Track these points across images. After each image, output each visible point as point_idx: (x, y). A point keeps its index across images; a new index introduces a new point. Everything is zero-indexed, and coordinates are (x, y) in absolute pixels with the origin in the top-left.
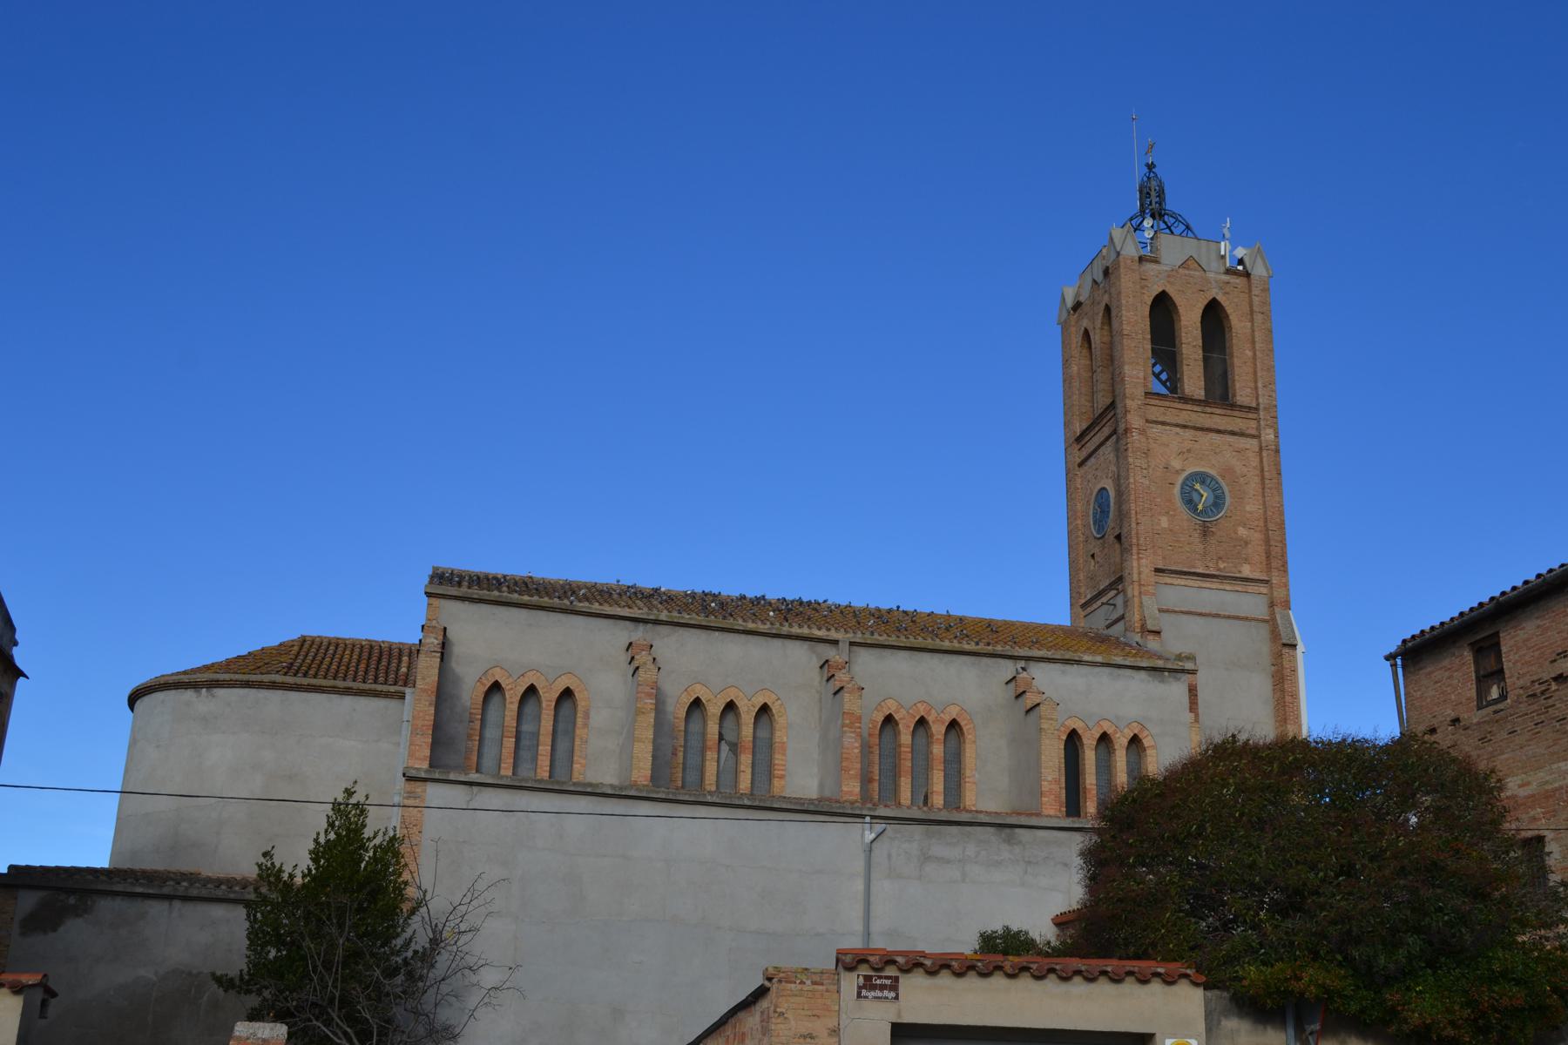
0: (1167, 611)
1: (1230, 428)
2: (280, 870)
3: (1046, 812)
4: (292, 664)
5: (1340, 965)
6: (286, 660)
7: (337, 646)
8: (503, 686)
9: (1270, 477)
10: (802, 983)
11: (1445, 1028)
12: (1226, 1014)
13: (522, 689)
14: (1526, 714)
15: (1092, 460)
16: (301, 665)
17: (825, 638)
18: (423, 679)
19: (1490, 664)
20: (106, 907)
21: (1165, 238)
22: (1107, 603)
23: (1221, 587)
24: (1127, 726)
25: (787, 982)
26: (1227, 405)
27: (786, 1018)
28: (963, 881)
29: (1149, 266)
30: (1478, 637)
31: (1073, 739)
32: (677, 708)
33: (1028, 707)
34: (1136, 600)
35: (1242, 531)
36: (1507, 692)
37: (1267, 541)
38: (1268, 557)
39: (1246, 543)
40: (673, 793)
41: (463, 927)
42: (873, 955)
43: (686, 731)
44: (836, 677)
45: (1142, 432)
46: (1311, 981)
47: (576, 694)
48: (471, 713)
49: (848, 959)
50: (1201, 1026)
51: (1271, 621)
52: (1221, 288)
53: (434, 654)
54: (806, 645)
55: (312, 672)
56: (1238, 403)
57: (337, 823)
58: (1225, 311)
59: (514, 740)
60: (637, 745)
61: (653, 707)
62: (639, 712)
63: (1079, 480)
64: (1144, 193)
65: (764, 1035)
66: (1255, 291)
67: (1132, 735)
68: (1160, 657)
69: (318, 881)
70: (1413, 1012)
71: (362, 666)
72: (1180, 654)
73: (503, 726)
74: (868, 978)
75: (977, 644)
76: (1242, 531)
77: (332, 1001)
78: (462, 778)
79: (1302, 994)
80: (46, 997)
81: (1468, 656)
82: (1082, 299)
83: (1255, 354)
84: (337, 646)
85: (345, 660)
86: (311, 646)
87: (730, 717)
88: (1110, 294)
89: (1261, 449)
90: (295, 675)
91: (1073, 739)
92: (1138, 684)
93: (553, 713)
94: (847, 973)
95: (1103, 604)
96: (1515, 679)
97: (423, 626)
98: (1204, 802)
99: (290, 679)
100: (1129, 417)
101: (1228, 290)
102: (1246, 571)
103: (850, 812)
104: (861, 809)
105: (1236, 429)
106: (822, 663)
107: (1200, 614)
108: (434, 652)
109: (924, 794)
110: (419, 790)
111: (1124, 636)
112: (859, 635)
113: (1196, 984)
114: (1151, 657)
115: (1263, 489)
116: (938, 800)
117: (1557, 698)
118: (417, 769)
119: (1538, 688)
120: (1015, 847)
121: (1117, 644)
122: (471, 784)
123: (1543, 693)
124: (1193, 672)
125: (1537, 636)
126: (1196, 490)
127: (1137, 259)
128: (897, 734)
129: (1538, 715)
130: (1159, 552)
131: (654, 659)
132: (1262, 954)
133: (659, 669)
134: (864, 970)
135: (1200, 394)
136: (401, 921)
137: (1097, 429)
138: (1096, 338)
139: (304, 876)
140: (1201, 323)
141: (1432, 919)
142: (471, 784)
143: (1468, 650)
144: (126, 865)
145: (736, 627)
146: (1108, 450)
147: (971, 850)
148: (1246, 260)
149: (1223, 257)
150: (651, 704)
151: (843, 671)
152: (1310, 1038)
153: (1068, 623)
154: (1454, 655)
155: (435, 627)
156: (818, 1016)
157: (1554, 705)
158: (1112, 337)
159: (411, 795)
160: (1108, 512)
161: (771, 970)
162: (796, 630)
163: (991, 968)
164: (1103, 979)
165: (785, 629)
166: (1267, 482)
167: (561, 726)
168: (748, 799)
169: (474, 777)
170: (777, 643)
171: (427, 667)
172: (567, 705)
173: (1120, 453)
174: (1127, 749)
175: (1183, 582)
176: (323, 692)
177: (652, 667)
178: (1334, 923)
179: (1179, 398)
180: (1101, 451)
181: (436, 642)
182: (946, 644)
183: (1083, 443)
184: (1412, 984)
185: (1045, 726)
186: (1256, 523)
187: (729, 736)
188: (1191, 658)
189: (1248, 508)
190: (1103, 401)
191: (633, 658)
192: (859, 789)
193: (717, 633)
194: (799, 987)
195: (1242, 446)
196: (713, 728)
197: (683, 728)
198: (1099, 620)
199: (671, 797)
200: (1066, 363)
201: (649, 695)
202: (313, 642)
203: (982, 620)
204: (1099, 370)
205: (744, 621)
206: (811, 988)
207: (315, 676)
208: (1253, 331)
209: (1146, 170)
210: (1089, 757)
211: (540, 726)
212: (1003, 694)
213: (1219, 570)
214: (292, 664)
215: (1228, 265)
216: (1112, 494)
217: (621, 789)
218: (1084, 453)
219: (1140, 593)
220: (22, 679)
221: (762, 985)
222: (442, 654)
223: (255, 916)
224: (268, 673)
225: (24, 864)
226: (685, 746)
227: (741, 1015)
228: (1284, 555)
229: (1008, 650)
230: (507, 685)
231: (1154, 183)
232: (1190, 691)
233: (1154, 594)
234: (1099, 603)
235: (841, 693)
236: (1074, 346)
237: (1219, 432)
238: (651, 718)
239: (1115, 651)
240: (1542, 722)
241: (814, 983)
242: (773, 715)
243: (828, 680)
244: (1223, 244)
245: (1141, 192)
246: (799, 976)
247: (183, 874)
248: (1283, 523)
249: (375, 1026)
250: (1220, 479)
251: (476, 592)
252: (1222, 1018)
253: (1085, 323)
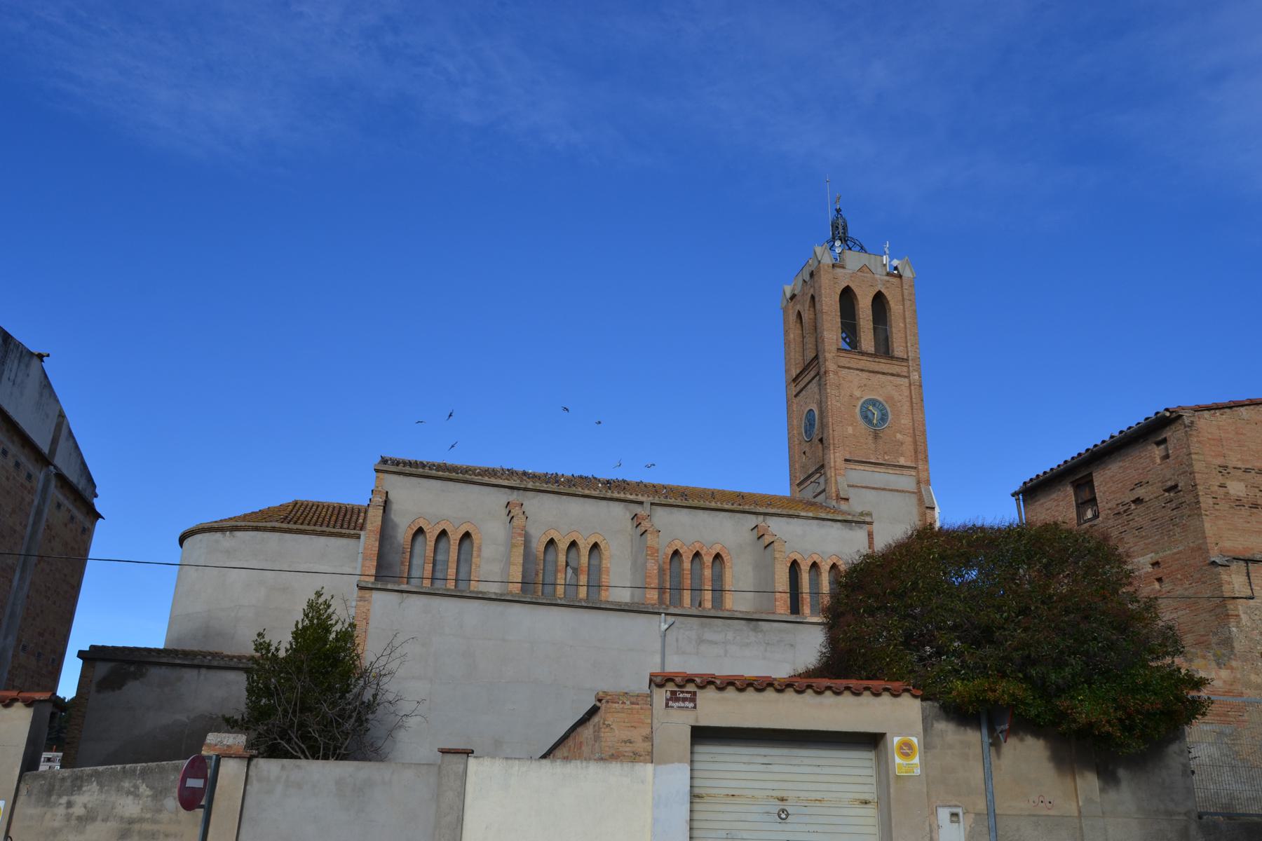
0: (853, 486)
1: (890, 371)
2: (269, 645)
3: (778, 612)
4: (287, 517)
5: (1020, 680)
6: (284, 514)
7: (318, 506)
8: (425, 530)
9: (916, 404)
10: (624, 703)
11: (1104, 725)
12: (937, 718)
13: (437, 532)
14: (1114, 527)
15: (804, 392)
16: (293, 517)
19: (1086, 495)
20: (155, 673)
21: (847, 253)
22: (814, 482)
23: (887, 471)
24: (829, 558)
25: (612, 702)
26: (889, 357)
27: (611, 728)
28: (725, 656)
29: (839, 270)
30: (1077, 477)
31: (794, 566)
32: (538, 545)
33: (766, 544)
34: (833, 479)
35: (899, 436)
36: (1099, 513)
37: (915, 442)
38: (916, 452)
39: (902, 443)
41: (383, 673)
42: (676, 677)
43: (544, 560)
44: (642, 525)
45: (836, 373)
46: (1003, 691)
47: (473, 536)
48: (404, 548)
49: (658, 680)
50: (919, 727)
51: (919, 493)
52: (884, 285)
54: (622, 504)
55: (300, 521)
56: (896, 356)
57: (310, 615)
58: (886, 299)
59: (432, 565)
60: (512, 567)
61: (523, 542)
62: (513, 546)
63: (795, 406)
64: (835, 227)
65: (596, 741)
66: (905, 287)
67: (832, 563)
68: (849, 514)
69: (295, 651)
70: (1080, 714)
71: (334, 518)
72: (862, 512)
73: (425, 557)
74: (673, 693)
75: (733, 505)
76: (899, 436)
77: (291, 726)
78: (396, 588)
79: (996, 702)
80: (55, 710)
81: (1070, 490)
82: (796, 292)
83: (905, 325)
84: (318, 506)
85: (323, 514)
86: (301, 506)
87: (573, 551)
88: (814, 287)
89: (910, 385)
90: (288, 523)
91: (794, 566)
92: (835, 531)
93: (457, 548)
94: (658, 689)
95: (811, 482)
96: (1104, 503)
97: (372, 491)
98: (916, 565)
99: (284, 525)
100: (827, 363)
101: (888, 285)
102: (902, 461)
104: (658, 609)
105: (895, 373)
106: (632, 516)
107: (874, 488)
109: (698, 601)
110: (367, 596)
111: (826, 503)
112: (657, 498)
113: (915, 696)
114: (843, 514)
115: (912, 409)
116: (708, 605)
117: (1136, 514)
118: (367, 582)
119: (1122, 509)
120: (759, 634)
121: (821, 507)
122: (402, 592)
123: (1125, 511)
124: (870, 523)
125: (1120, 473)
126: (870, 410)
127: (831, 265)
128: (681, 562)
129: (1122, 527)
130: (847, 449)
131: (524, 512)
132: (963, 674)
133: (527, 518)
134: (671, 687)
135: (872, 350)
136: (353, 680)
137: (806, 373)
138: (805, 316)
139: (287, 651)
140: (872, 305)
141: (1089, 646)
142: (402, 592)
143: (1069, 486)
144: (170, 647)
145: (577, 493)
146: (814, 384)
147: (730, 636)
148: (899, 267)
149: (885, 265)
151: (647, 520)
152: (1000, 735)
153: (789, 495)
154: (1060, 490)
156: (635, 727)
157: (1134, 519)
158: (815, 315)
159: (361, 599)
160: (814, 424)
161: (601, 694)
162: (616, 495)
163: (765, 685)
164: (847, 693)
165: (609, 494)
166: (914, 405)
167: (462, 557)
169: (404, 587)
170: (604, 503)
171: (374, 516)
172: (467, 543)
173: (822, 387)
174: (830, 572)
175: (862, 468)
176: (307, 534)
177: (522, 516)
178: (1016, 649)
179: (859, 352)
180: (809, 386)
181: (381, 500)
182: (713, 505)
183: (797, 382)
184: (1075, 695)
185: (777, 556)
186: (908, 431)
187: (572, 563)
188: (869, 514)
189: (903, 422)
190: (811, 355)
191: (510, 512)
192: (657, 596)
193: (565, 497)
194: (622, 706)
195: (898, 383)
196: (562, 558)
197: (542, 558)
198: (808, 493)
199: (534, 600)
200: (786, 333)
201: (520, 535)
202: (302, 504)
203: (735, 492)
204: (807, 336)
205: (582, 489)
206: (629, 707)
207: (302, 524)
208: (904, 311)
209: (836, 213)
210: (805, 578)
211: (449, 556)
212: (750, 537)
213: (885, 460)
214: (287, 517)
215: (888, 270)
216: (816, 413)
217: (501, 595)
218: (798, 388)
219: (835, 474)
220: (100, 519)
221: (595, 705)
222: (384, 507)
223: (252, 678)
224: (271, 521)
225: (101, 645)
226: (544, 570)
227: (579, 730)
228: (926, 451)
229: (752, 508)
231: (840, 221)
232: (869, 535)
233: (844, 475)
234: (809, 482)
235: (645, 535)
236: (791, 323)
237: (884, 374)
238: (521, 549)
239: (821, 511)
240: (1125, 531)
241: (632, 703)
242: (601, 550)
243: (637, 527)
244: (885, 257)
245: (832, 226)
246: (621, 698)
247: (210, 653)
248: (925, 431)
249: (322, 743)
250: (885, 403)
251: (408, 469)
252: (934, 722)
253: (798, 307)
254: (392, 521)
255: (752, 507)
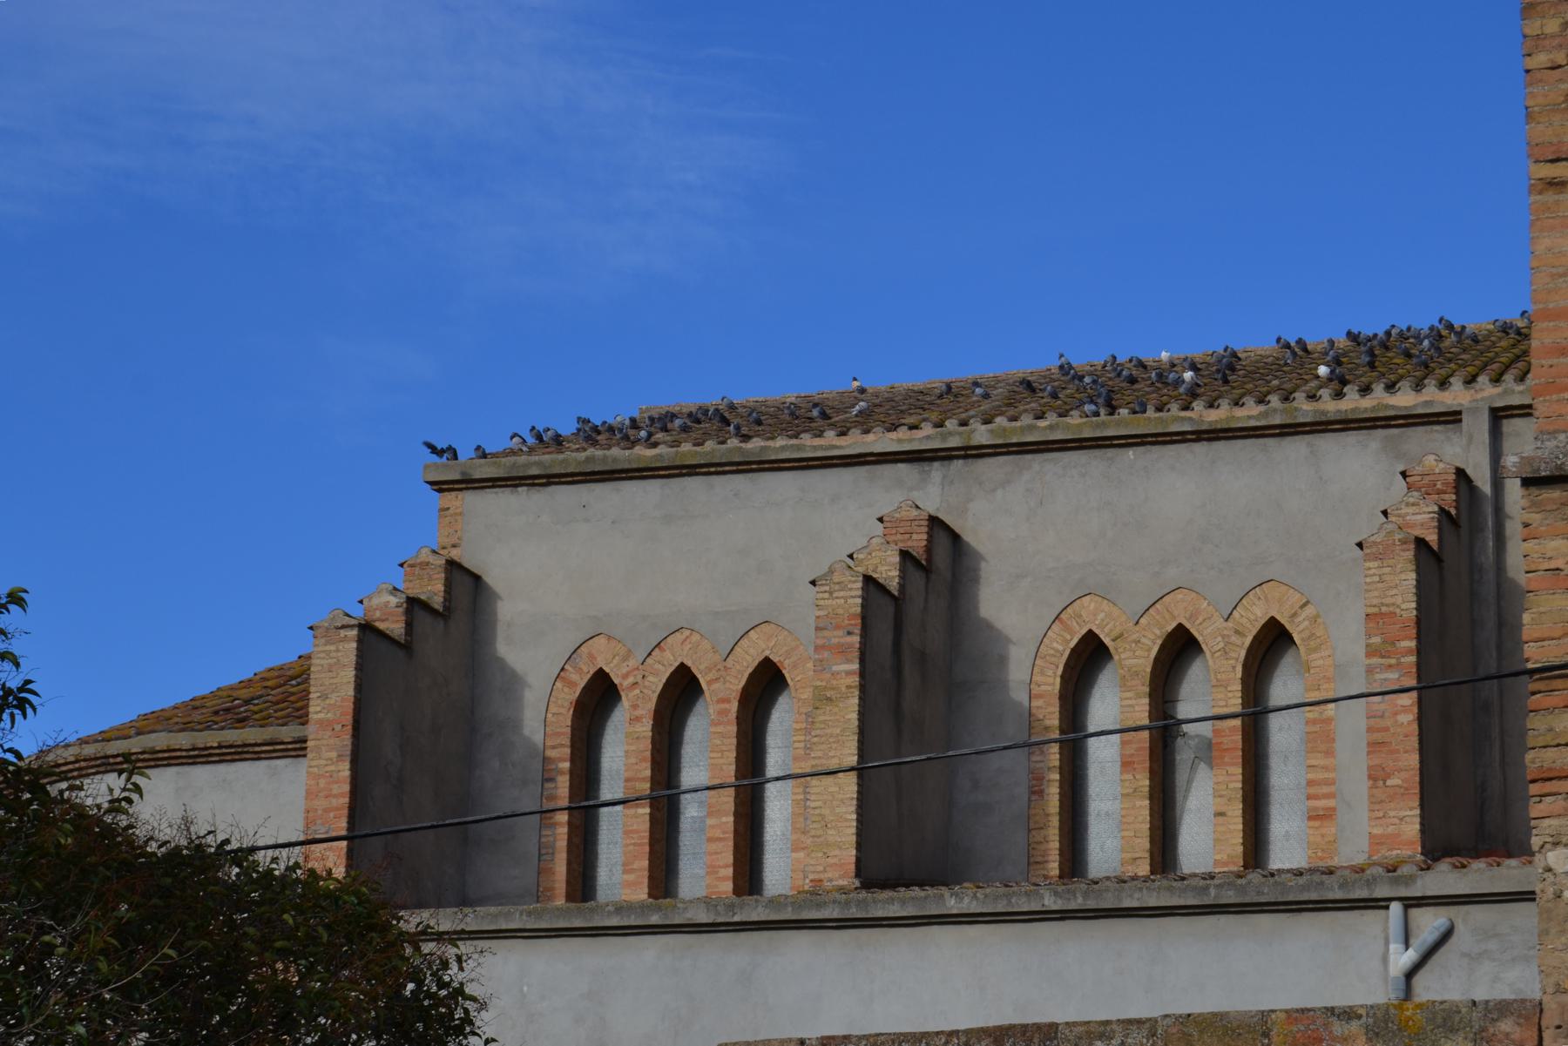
17: (1420, 411)
18: (324, 697)
40: (859, 903)
53: (343, 633)
61: (855, 680)
103: (1339, 895)
108: (343, 627)
150: (848, 673)
155: (428, 564)
168: (1056, 894)
170: (1296, 447)
193: (1131, 453)
230: (625, 676)
254: (502, 664)
255: (1026, 420)
